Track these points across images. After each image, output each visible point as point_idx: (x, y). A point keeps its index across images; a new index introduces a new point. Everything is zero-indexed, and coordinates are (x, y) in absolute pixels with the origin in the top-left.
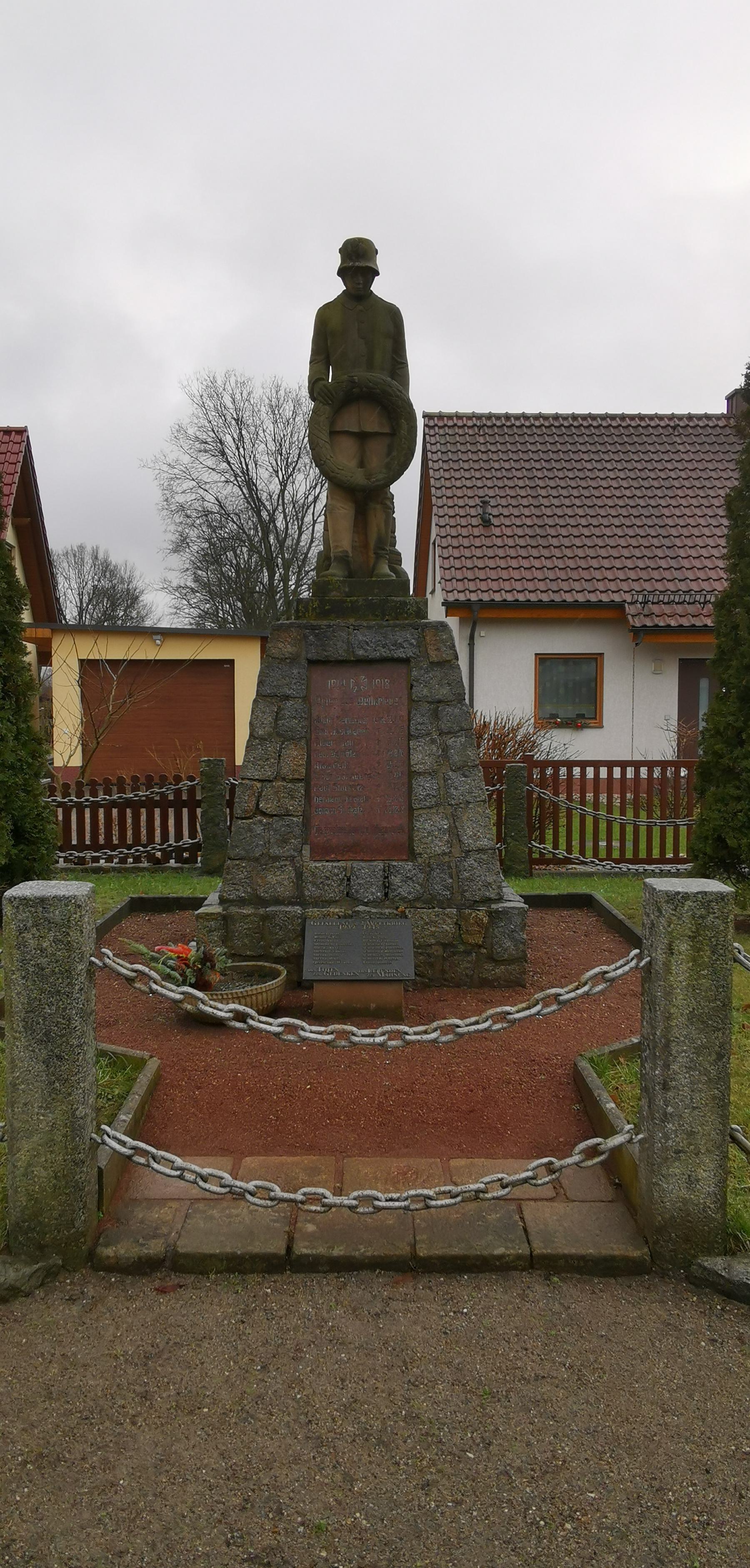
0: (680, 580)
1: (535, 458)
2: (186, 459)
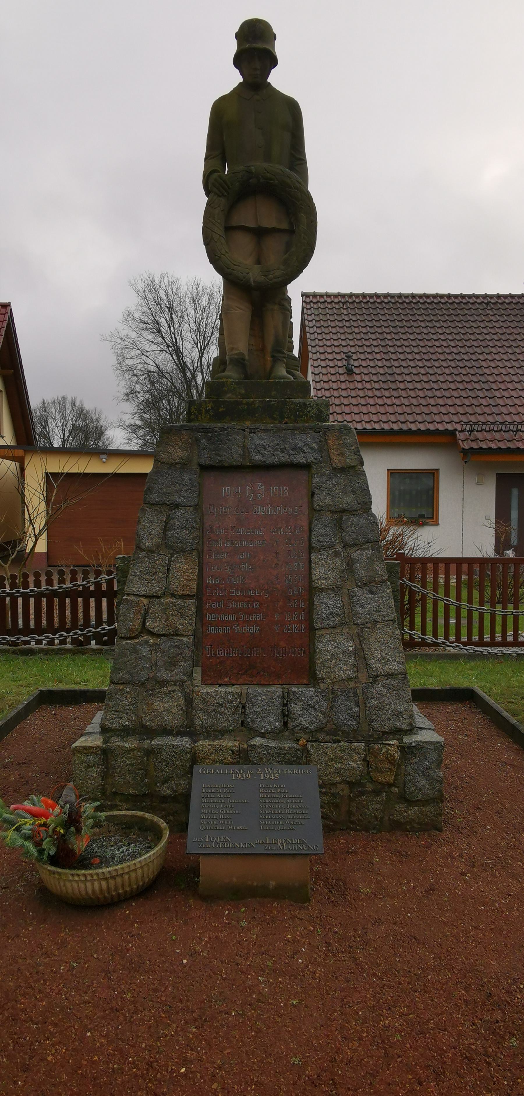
0: (497, 414)
1: (385, 325)
2: (133, 335)
